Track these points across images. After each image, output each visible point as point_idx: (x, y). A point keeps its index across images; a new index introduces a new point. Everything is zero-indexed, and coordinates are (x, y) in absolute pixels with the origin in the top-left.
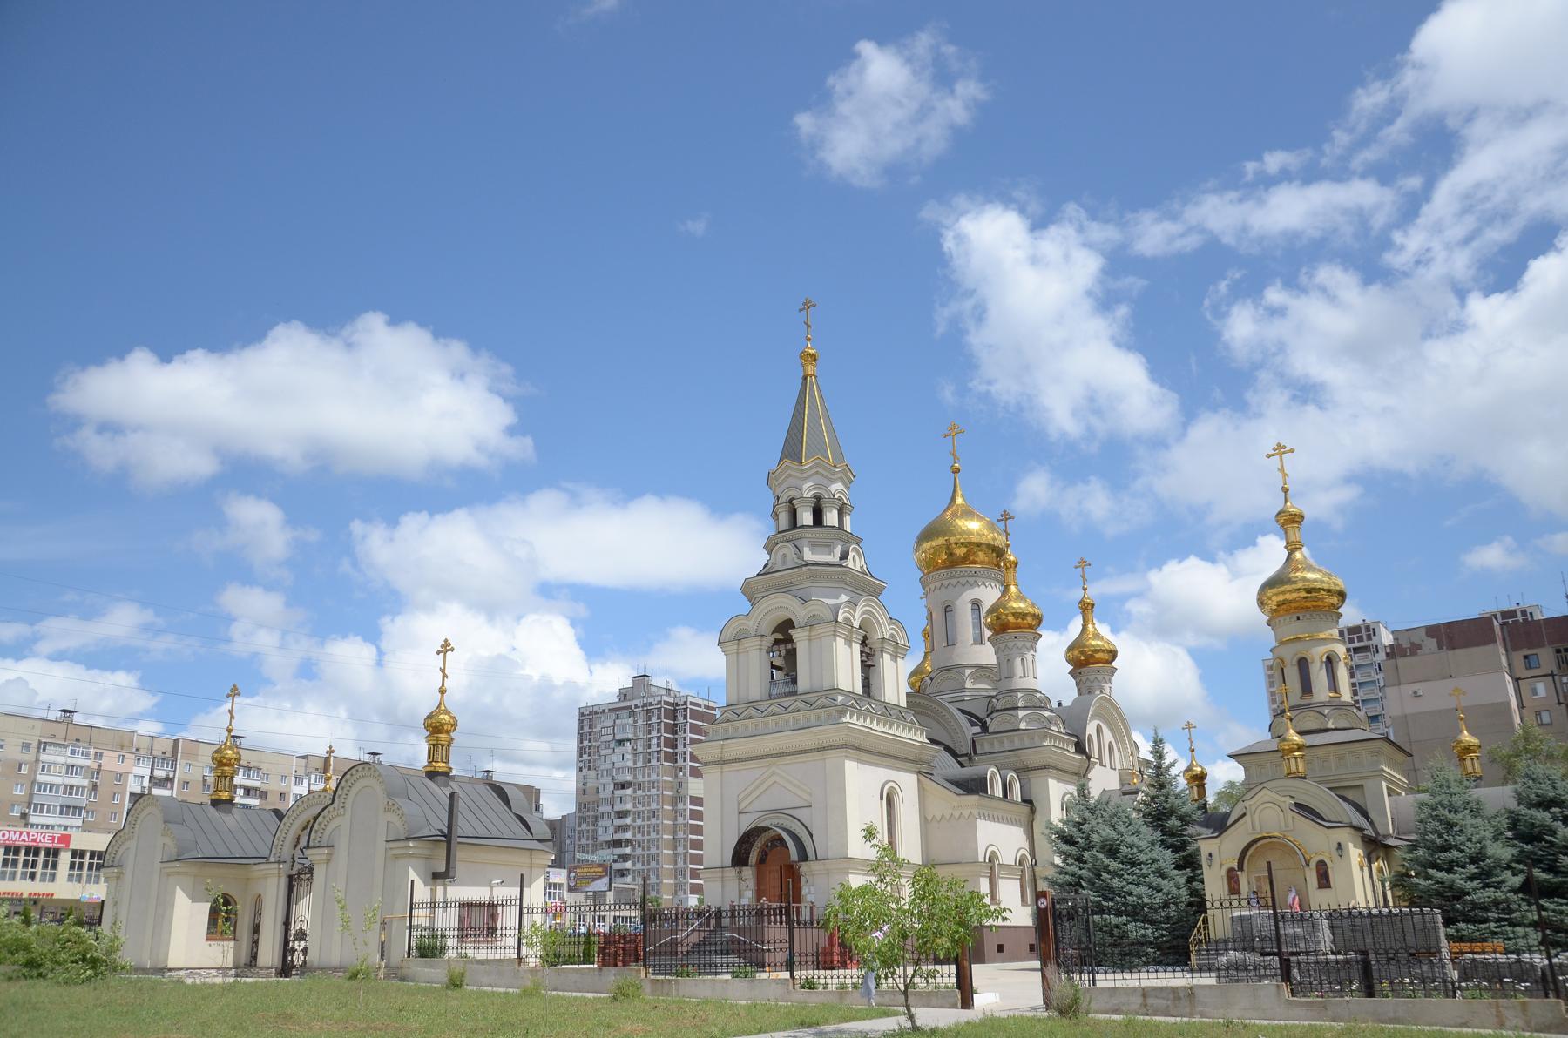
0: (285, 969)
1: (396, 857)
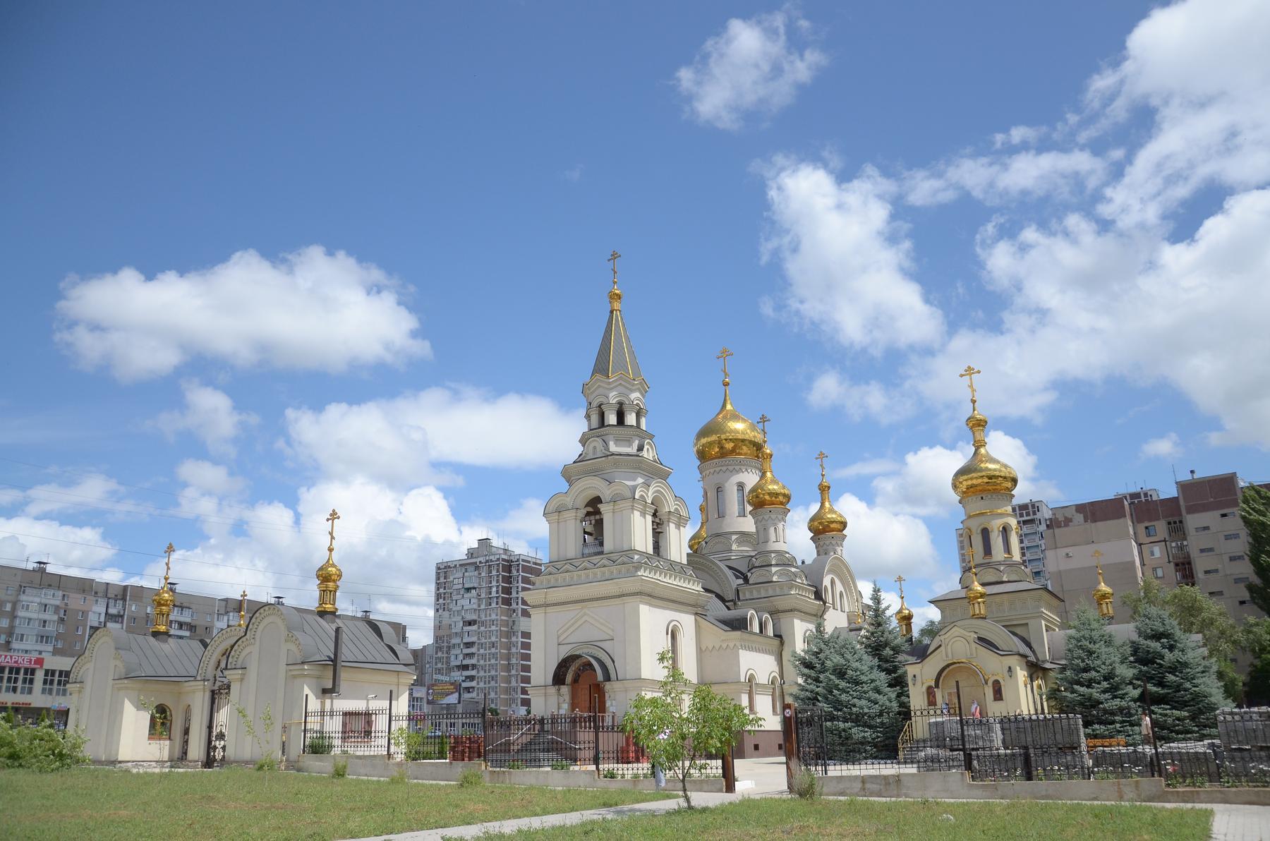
0: (209, 762)
1: (295, 677)
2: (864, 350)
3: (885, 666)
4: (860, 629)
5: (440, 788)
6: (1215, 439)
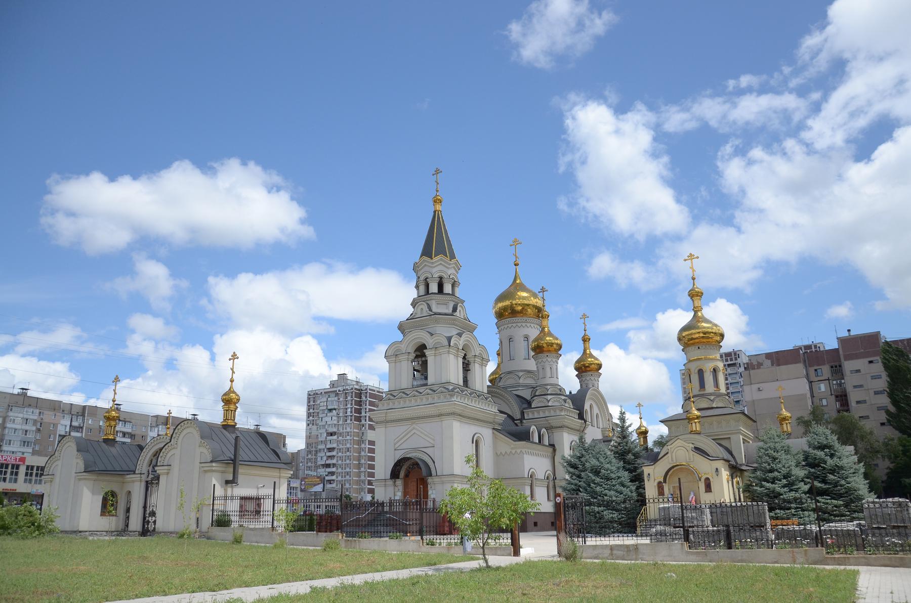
0: (144, 532)
1: (205, 471)
2: (632, 236)
4: (610, 441)
5: (308, 552)
6: (879, 306)
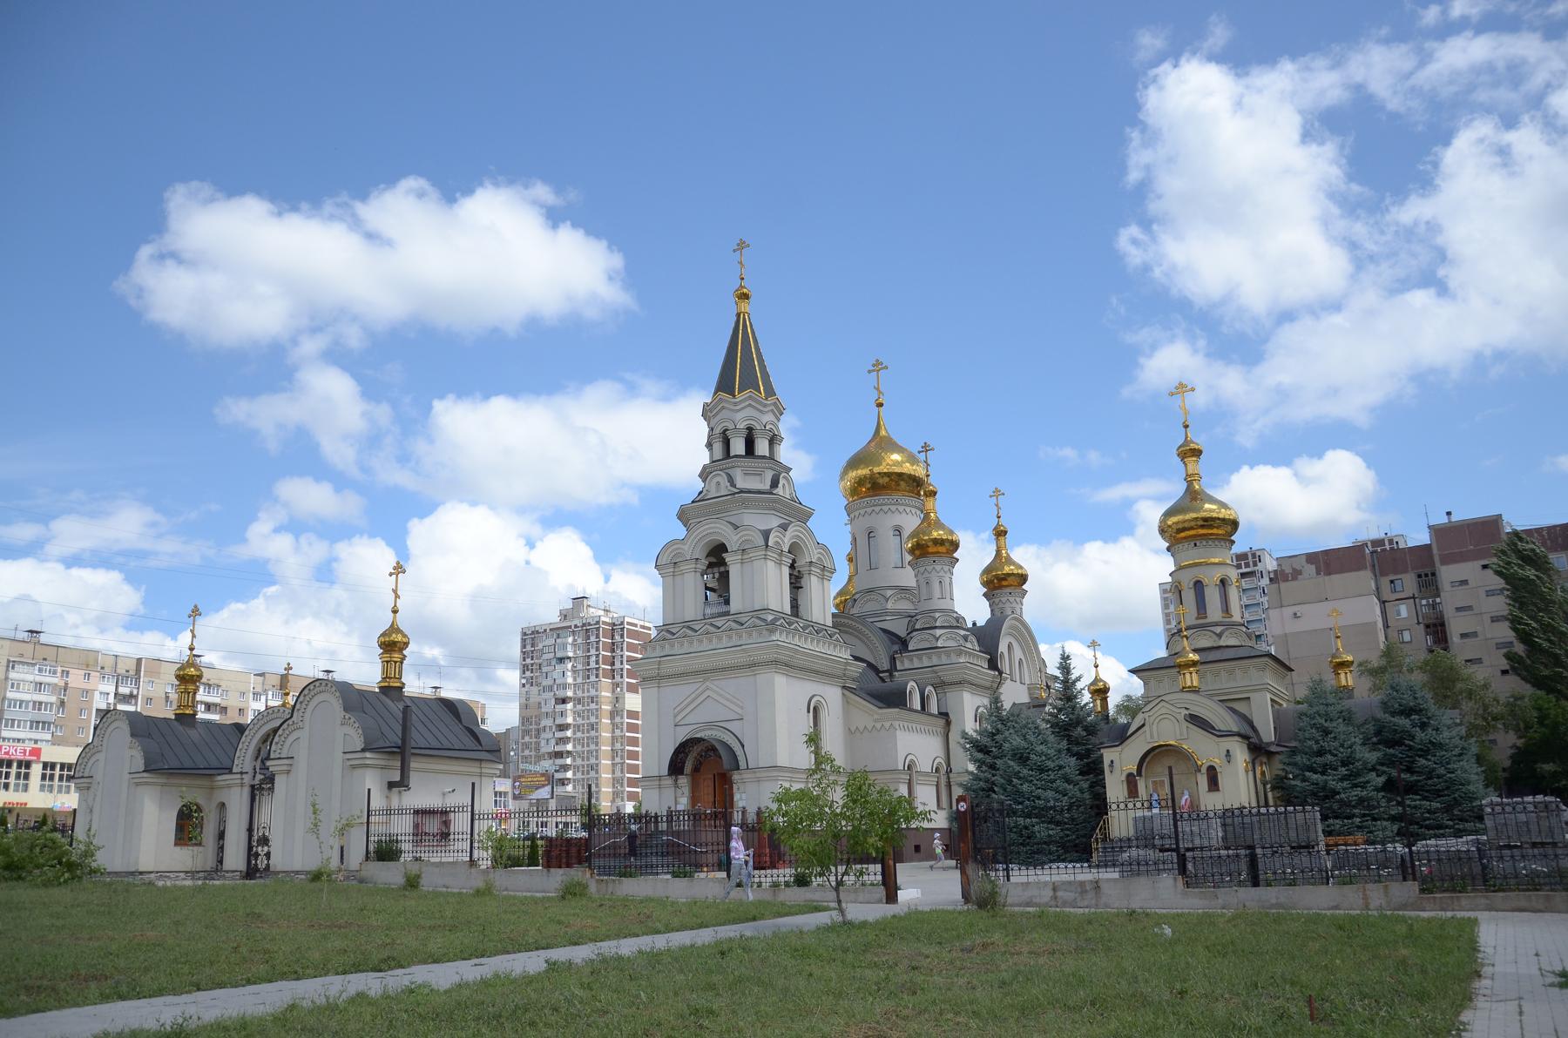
0: (251, 872)
1: (354, 767)
3: (1075, 749)
